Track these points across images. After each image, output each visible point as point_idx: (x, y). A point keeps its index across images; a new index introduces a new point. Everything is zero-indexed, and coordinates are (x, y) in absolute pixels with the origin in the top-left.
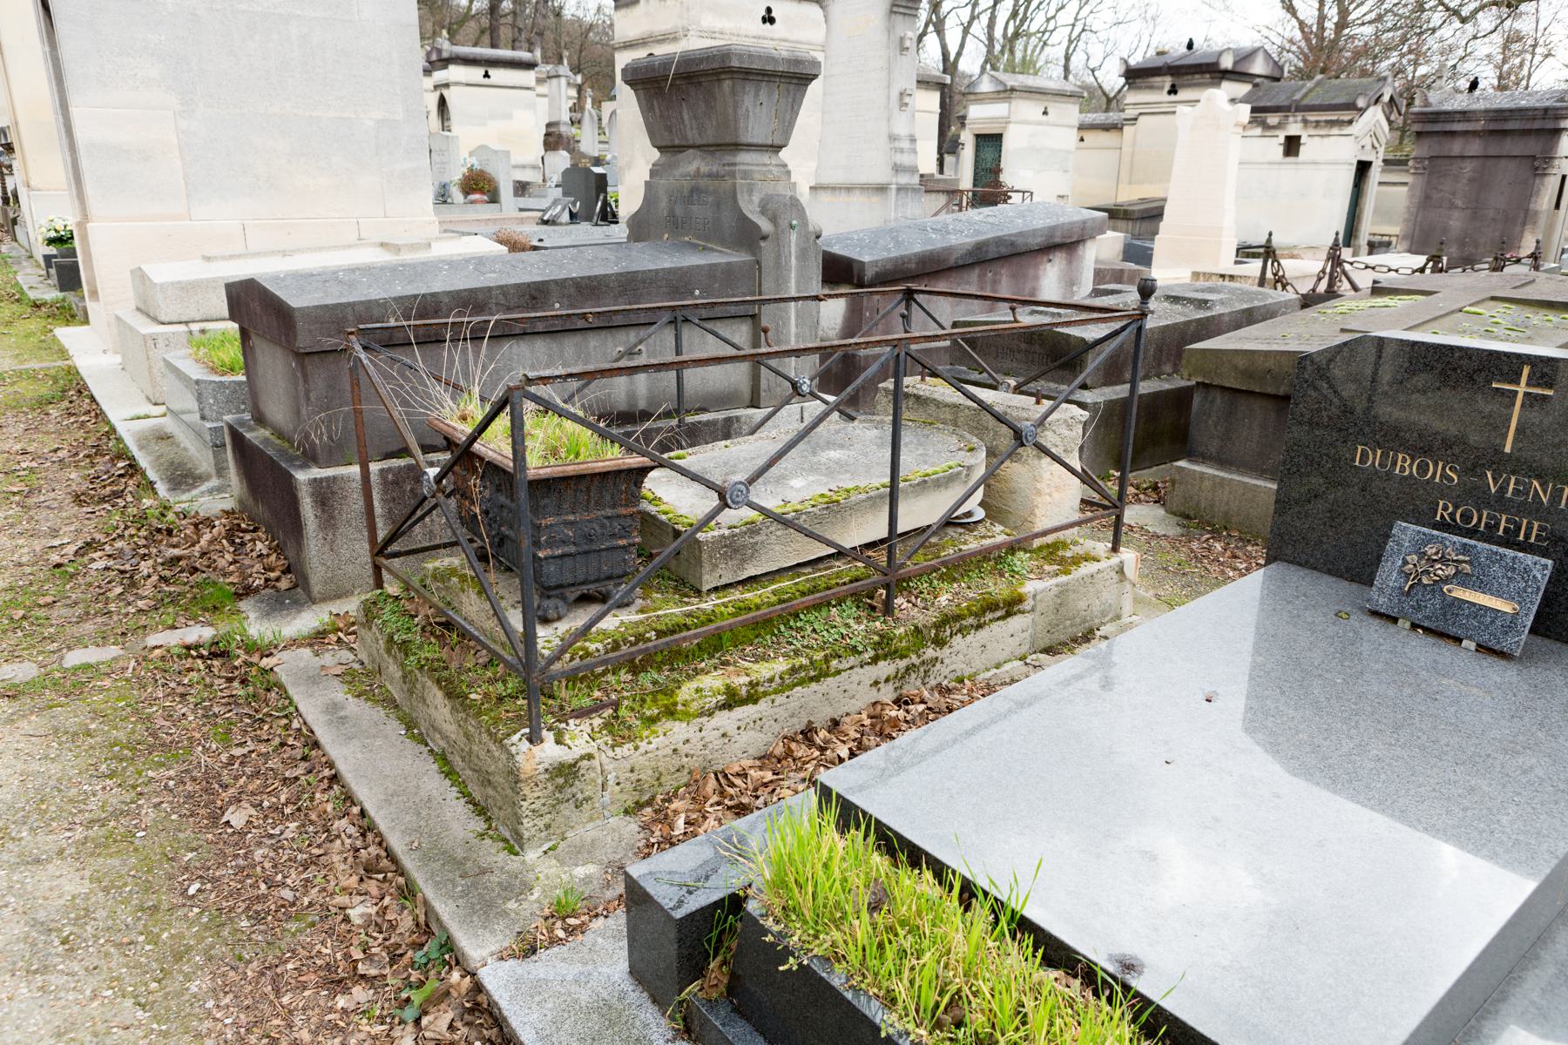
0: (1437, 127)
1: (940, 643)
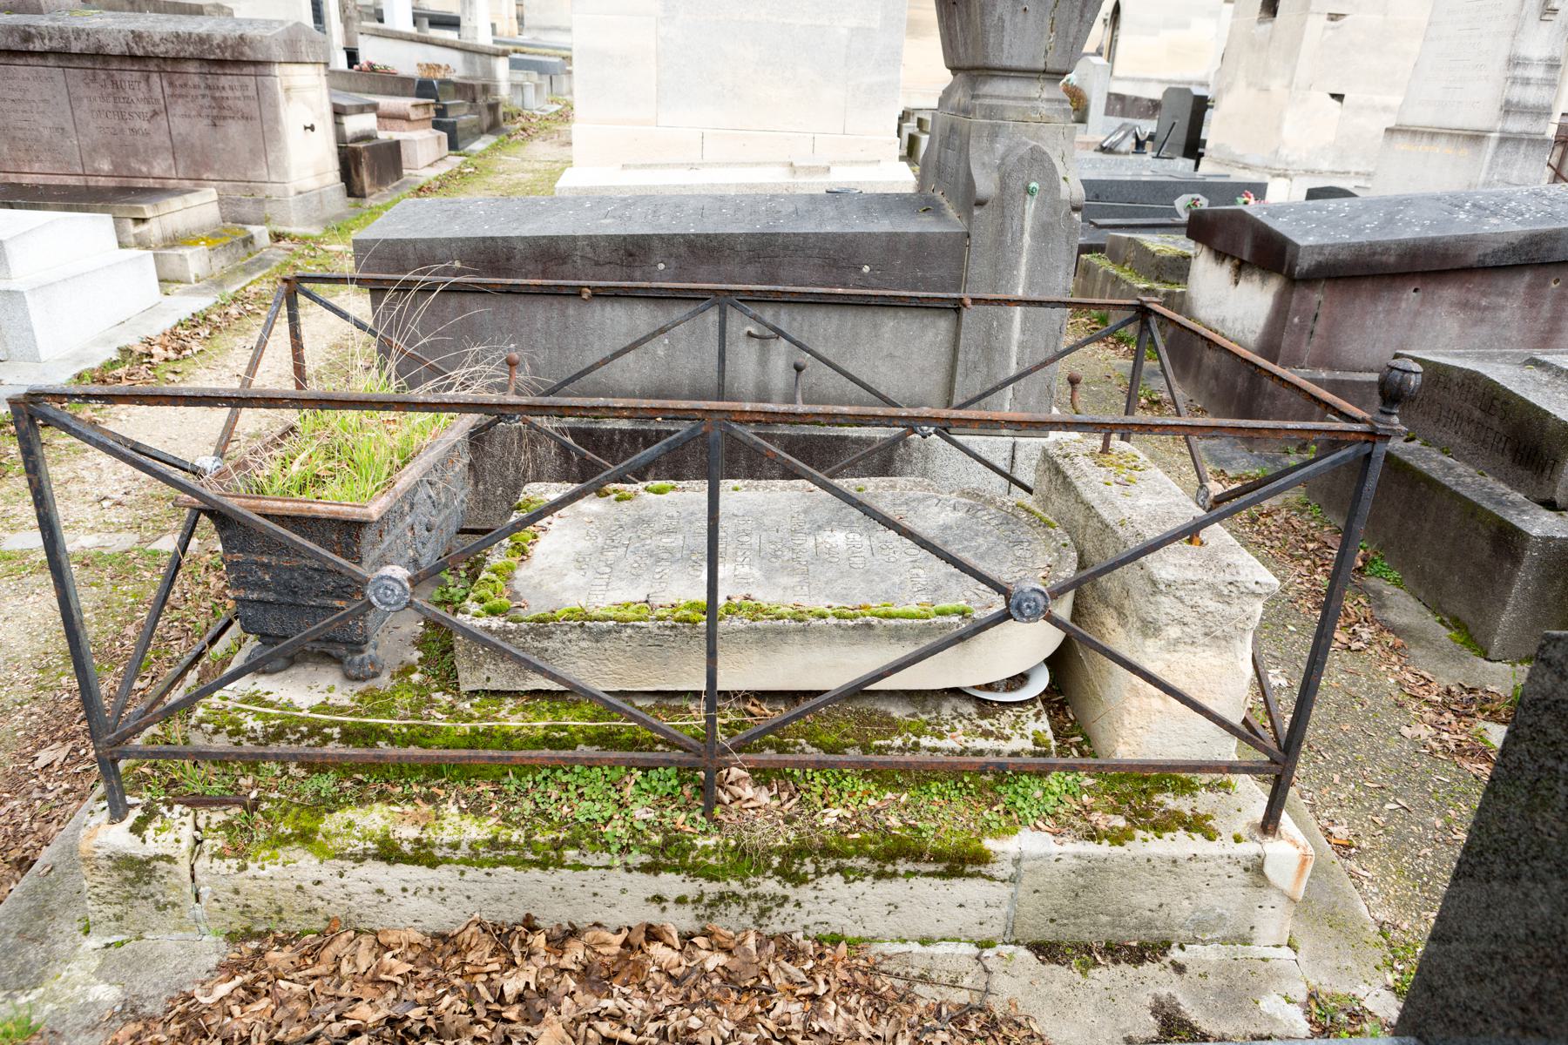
1: (790, 876)
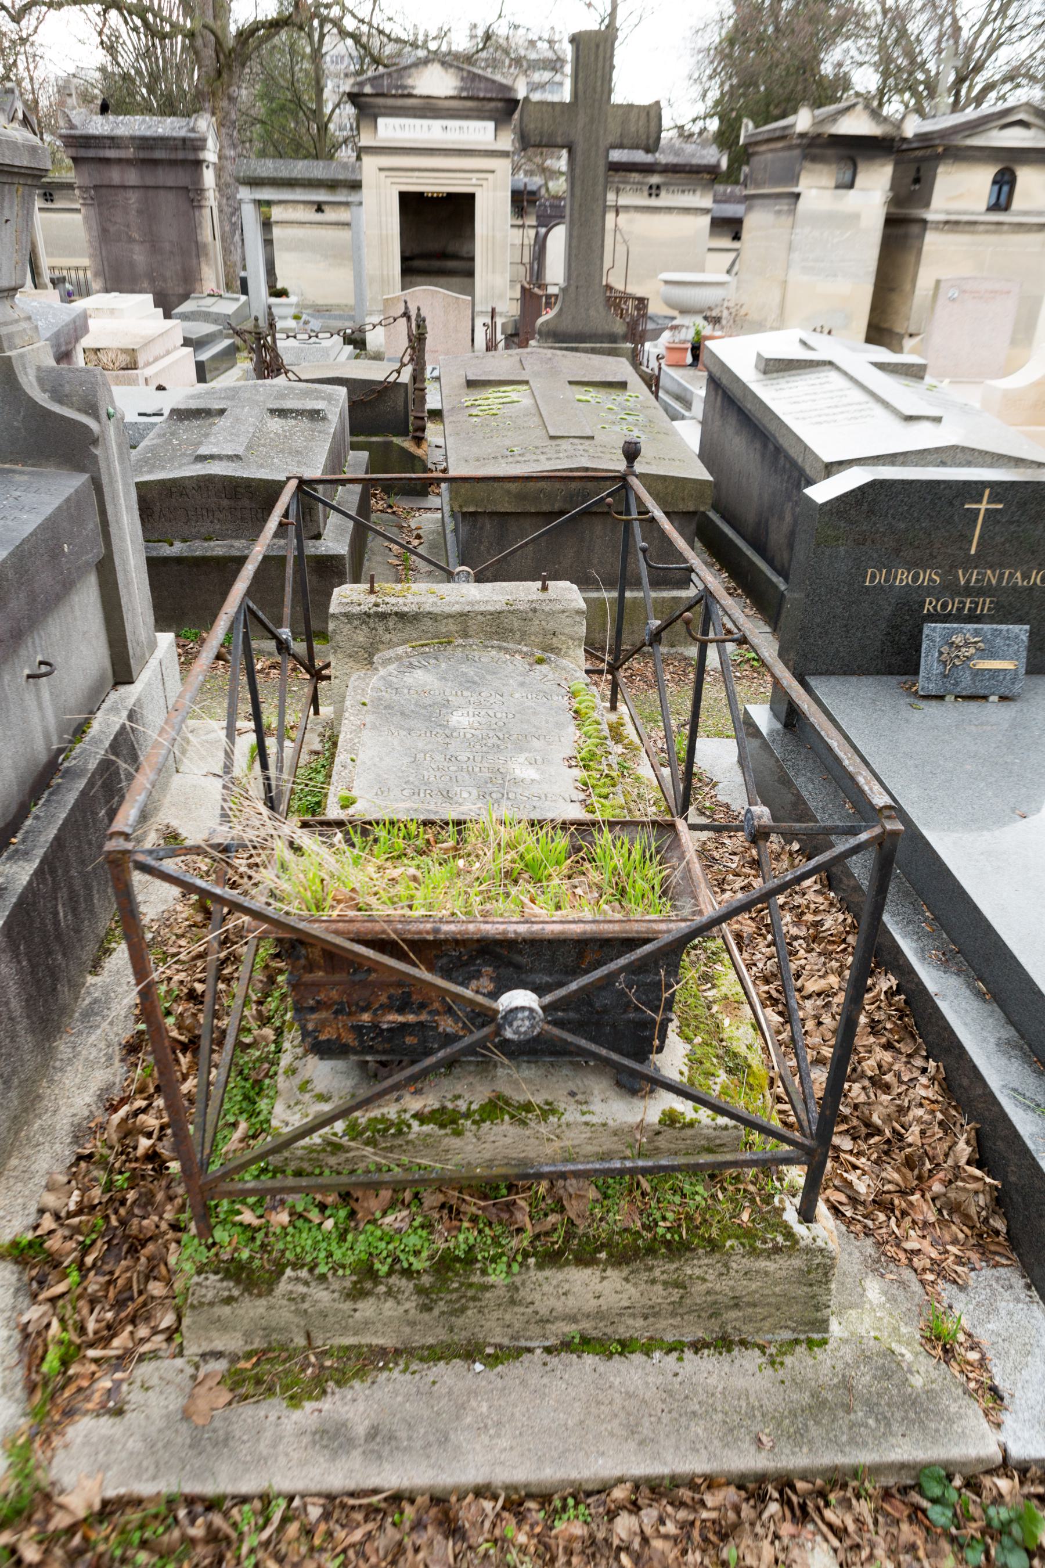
0: (91, 153)
